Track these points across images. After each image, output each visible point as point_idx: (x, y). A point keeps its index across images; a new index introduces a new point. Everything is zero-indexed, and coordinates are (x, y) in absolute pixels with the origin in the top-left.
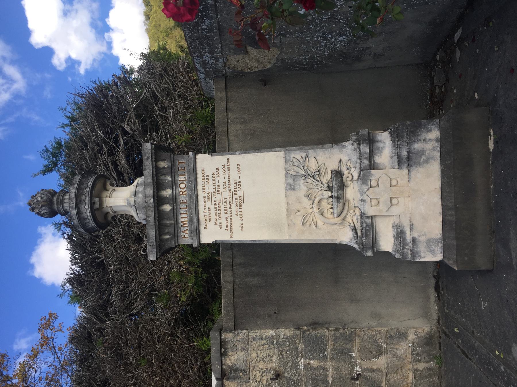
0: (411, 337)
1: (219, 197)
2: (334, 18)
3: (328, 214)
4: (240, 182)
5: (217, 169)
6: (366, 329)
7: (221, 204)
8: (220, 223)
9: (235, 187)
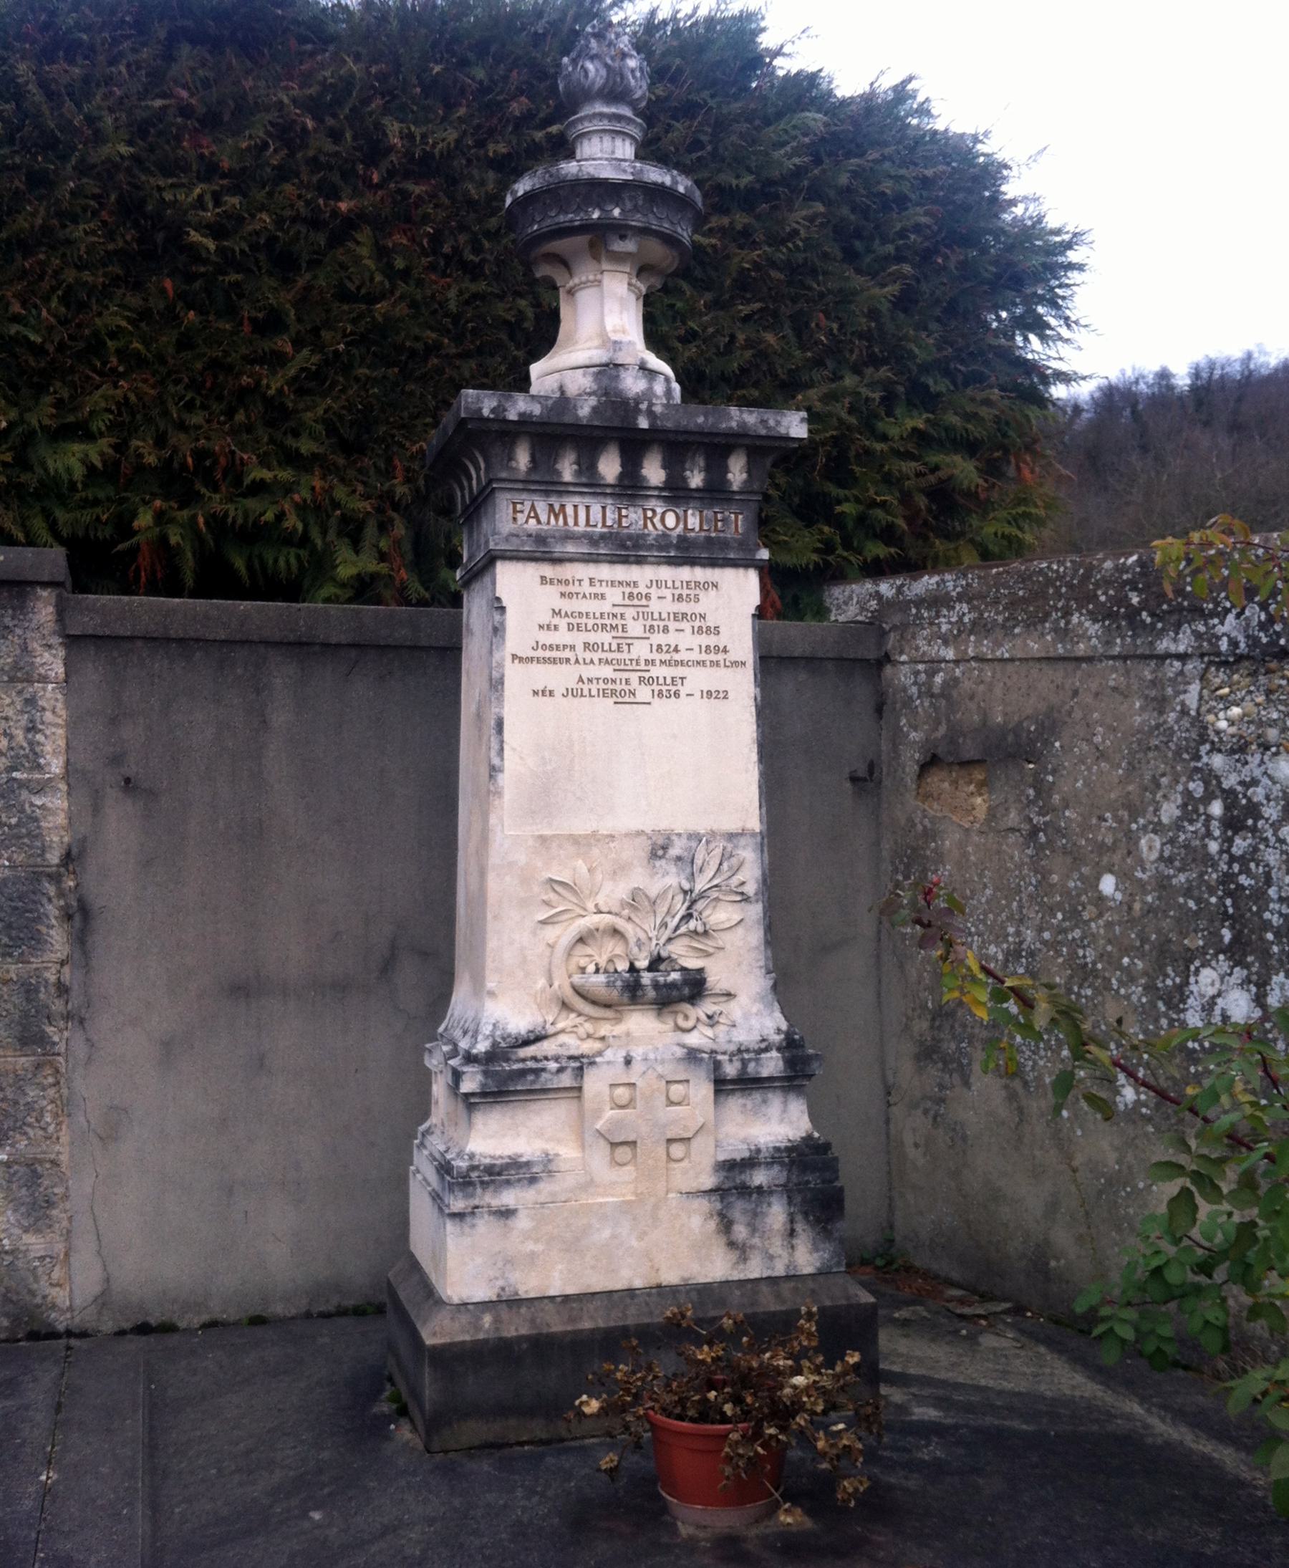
0: (35, 1244)
1: (635, 628)
2: (1085, 979)
3: (583, 957)
4: (677, 695)
5: (717, 631)
6: (65, 1091)
7: (614, 634)
8: (556, 628)
9: (661, 681)
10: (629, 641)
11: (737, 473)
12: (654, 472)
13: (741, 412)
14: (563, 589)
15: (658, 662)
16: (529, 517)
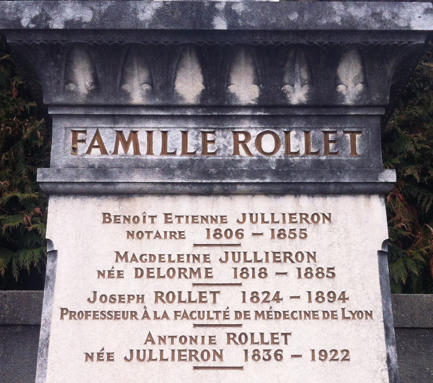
1: (223, 273)
5: (331, 273)
7: (195, 280)
8: (120, 274)
9: (257, 338)
10: (215, 289)
11: (350, 84)
12: (244, 88)
13: (347, 6)
14: (131, 227)
15: (252, 315)
16: (92, 146)
